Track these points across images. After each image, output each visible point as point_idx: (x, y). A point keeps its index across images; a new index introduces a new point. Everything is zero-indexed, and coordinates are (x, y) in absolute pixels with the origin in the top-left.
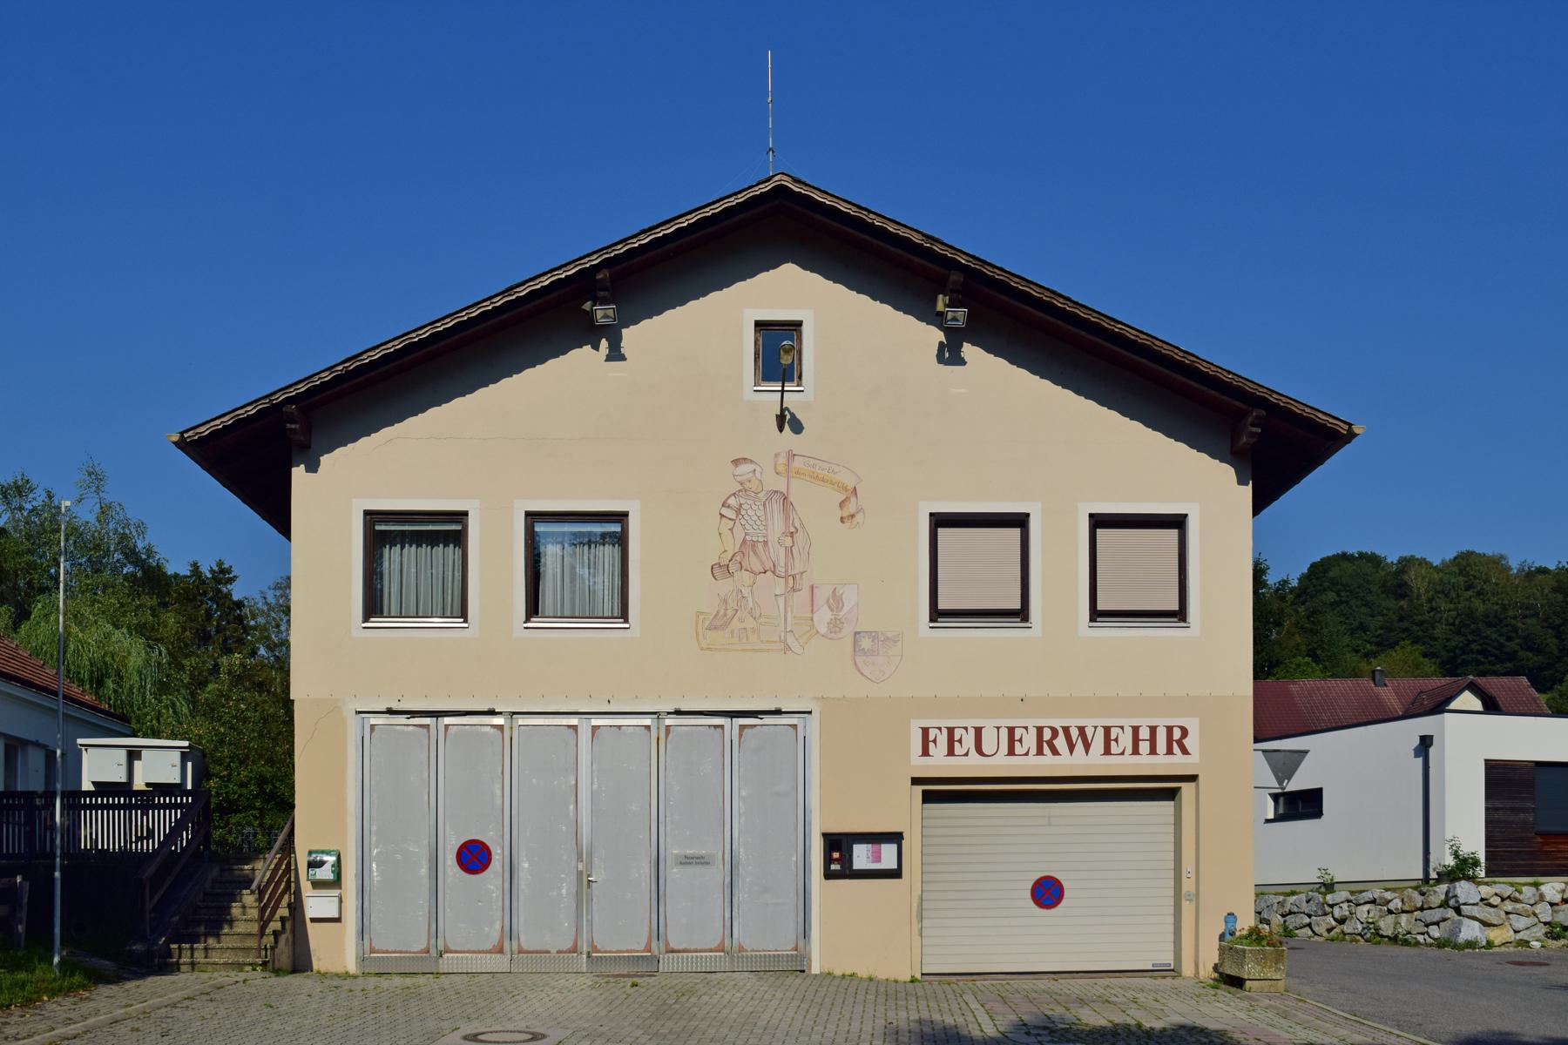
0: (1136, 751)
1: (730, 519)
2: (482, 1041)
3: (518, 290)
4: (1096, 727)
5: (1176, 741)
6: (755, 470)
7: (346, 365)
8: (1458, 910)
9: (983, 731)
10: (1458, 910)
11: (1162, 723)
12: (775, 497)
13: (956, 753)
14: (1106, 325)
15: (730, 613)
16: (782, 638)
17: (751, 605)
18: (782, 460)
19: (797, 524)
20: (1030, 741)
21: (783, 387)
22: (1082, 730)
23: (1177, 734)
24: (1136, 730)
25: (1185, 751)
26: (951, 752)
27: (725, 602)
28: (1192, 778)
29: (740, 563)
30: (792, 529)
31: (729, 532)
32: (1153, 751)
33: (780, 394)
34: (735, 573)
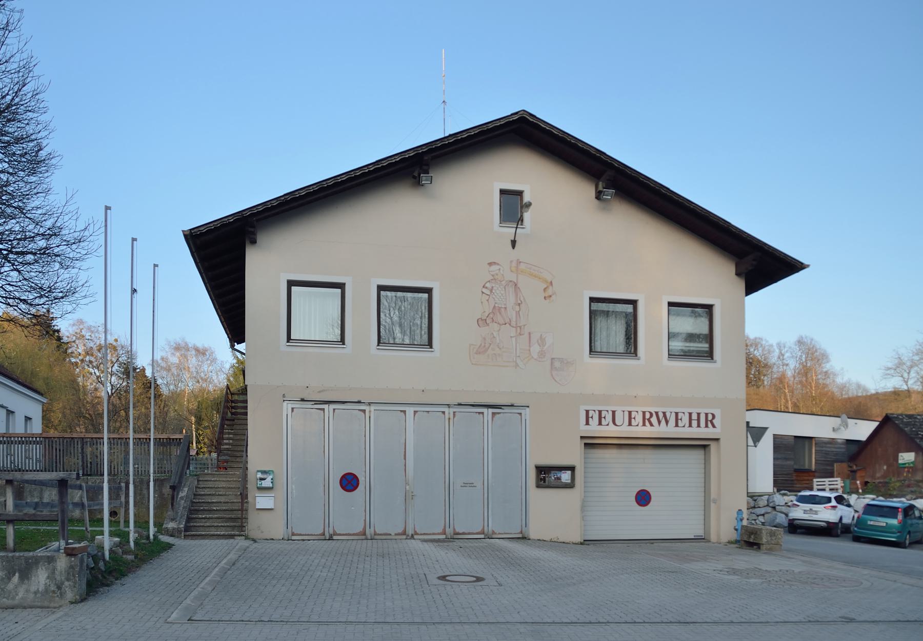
0: (690, 426)
1: (488, 295)
2: (448, 581)
3: (383, 162)
4: (671, 412)
5: (710, 421)
6: (500, 269)
7: (286, 197)
8: (774, 508)
9: (616, 412)
10: (774, 508)
11: (703, 411)
12: (511, 284)
13: (633, 424)
14: (687, 204)
15: (487, 345)
16: (515, 359)
17: (498, 342)
18: (514, 264)
19: (522, 299)
20: (639, 418)
21: (517, 225)
22: (664, 413)
23: (710, 417)
24: (690, 414)
25: (714, 426)
26: (600, 424)
27: (485, 339)
28: (717, 440)
29: (492, 318)
30: (519, 302)
31: (487, 302)
32: (699, 426)
33: (515, 229)
34: (490, 324)
